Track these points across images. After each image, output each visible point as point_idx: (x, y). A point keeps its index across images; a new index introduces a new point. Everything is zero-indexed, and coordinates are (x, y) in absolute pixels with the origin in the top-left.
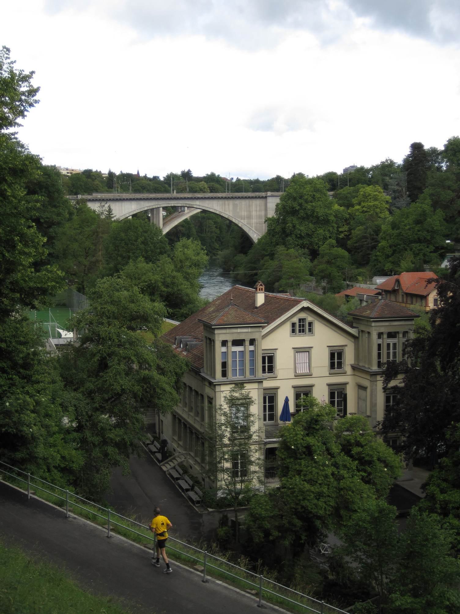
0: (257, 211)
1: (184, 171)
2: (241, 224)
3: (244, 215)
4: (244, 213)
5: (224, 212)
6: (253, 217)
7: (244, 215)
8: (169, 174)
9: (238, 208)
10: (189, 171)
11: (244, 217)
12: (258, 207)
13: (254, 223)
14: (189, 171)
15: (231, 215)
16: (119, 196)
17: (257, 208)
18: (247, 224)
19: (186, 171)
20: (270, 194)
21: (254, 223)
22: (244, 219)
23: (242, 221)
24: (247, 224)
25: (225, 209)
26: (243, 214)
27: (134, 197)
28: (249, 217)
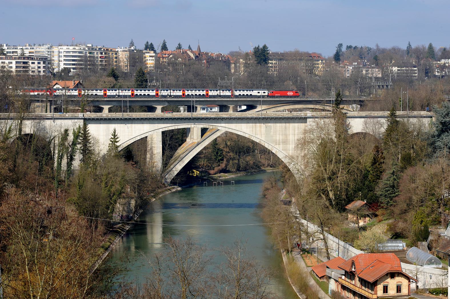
0: (295, 134)
1: (258, 48)
2: (276, 150)
3: (279, 140)
4: (279, 137)
5: (254, 135)
6: (291, 143)
7: (279, 140)
8: (285, 51)
9: (272, 130)
10: (265, 47)
11: (279, 142)
12: (296, 129)
13: (291, 149)
14: (265, 47)
15: (263, 139)
16: (95, 116)
17: (295, 131)
18: (282, 150)
19: (261, 47)
20: (310, 115)
21: (291, 149)
22: (279, 144)
23: (277, 146)
24: (282, 150)
25: (256, 133)
26: (278, 138)
27: (146, 117)
28: (285, 142)
